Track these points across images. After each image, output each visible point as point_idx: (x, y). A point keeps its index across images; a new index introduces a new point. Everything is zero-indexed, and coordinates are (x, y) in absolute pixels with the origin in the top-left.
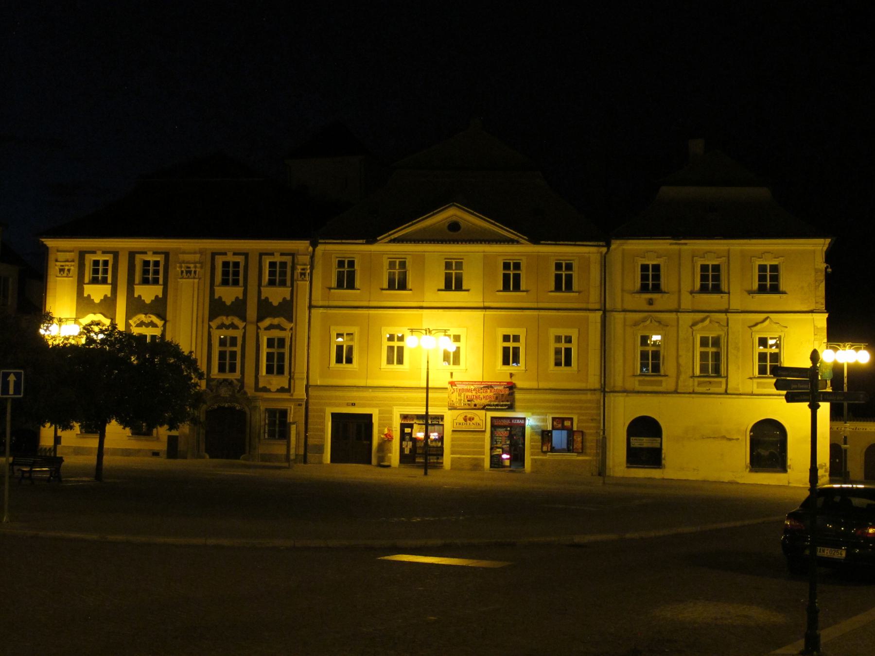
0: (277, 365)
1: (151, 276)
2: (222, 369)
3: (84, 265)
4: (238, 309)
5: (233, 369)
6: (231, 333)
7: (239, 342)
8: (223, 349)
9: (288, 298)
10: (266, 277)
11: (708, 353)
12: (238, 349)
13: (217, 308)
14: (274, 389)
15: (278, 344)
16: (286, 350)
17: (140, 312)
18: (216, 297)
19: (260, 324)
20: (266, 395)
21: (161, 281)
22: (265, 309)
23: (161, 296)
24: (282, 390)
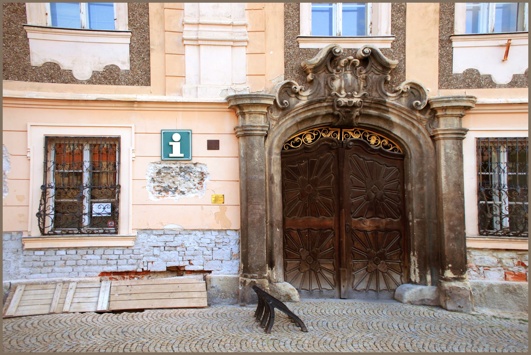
14: (83, 72)
20: (483, 96)
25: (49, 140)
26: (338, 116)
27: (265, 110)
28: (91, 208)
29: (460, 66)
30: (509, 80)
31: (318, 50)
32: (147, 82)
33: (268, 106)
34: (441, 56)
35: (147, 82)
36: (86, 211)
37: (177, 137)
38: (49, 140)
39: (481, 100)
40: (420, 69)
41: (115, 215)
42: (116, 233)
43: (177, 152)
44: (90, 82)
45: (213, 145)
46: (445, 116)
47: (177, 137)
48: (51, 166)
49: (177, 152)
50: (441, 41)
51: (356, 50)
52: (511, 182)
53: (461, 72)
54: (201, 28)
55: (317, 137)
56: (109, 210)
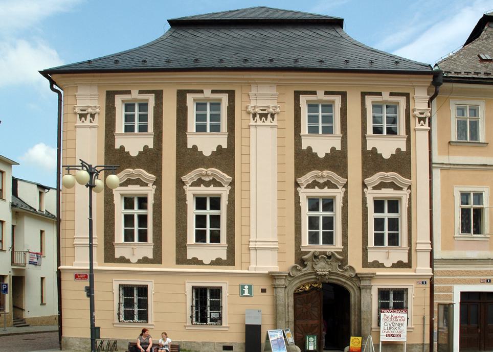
0: (389, 233)
1: (385, 126)
2: (313, 239)
3: (186, 109)
4: (336, 161)
5: (329, 239)
6: (327, 192)
7: (224, 203)
8: (129, 212)
9: (404, 149)
10: (370, 125)
11: (212, 208)
12: (223, 212)
13: (305, 161)
14: (388, 264)
15: (318, 204)
16: (223, 212)
17: (315, 168)
18: (304, 147)
19: (367, 180)
20: (379, 272)
21: (151, 129)
22: (372, 161)
23: (225, 146)
24: (399, 265)
25: (193, 287)
26: (318, 279)
27: (285, 277)
28: (210, 315)
29: (370, 260)
30: (137, 261)
31: (309, 252)
32: (233, 264)
33: (286, 276)
34: (363, 255)
35: (233, 264)
36: (209, 316)
37: (246, 287)
38: (193, 287)
39: (377, 273)
40: (355, 260)
41: (220, 318)
42: (221, 325)
43: (246, 293)
44: (137, 263)
45: (264, 291)
46: (363, 280)
47: (246, 287)
48: (194, 297)
49: (246, 293)
50: (363, 249)
51: (326, 252)
52: (139, 312)
53: (118, 257)
54: (257, 243)
55: (311, 286)
56: (218, 316)
